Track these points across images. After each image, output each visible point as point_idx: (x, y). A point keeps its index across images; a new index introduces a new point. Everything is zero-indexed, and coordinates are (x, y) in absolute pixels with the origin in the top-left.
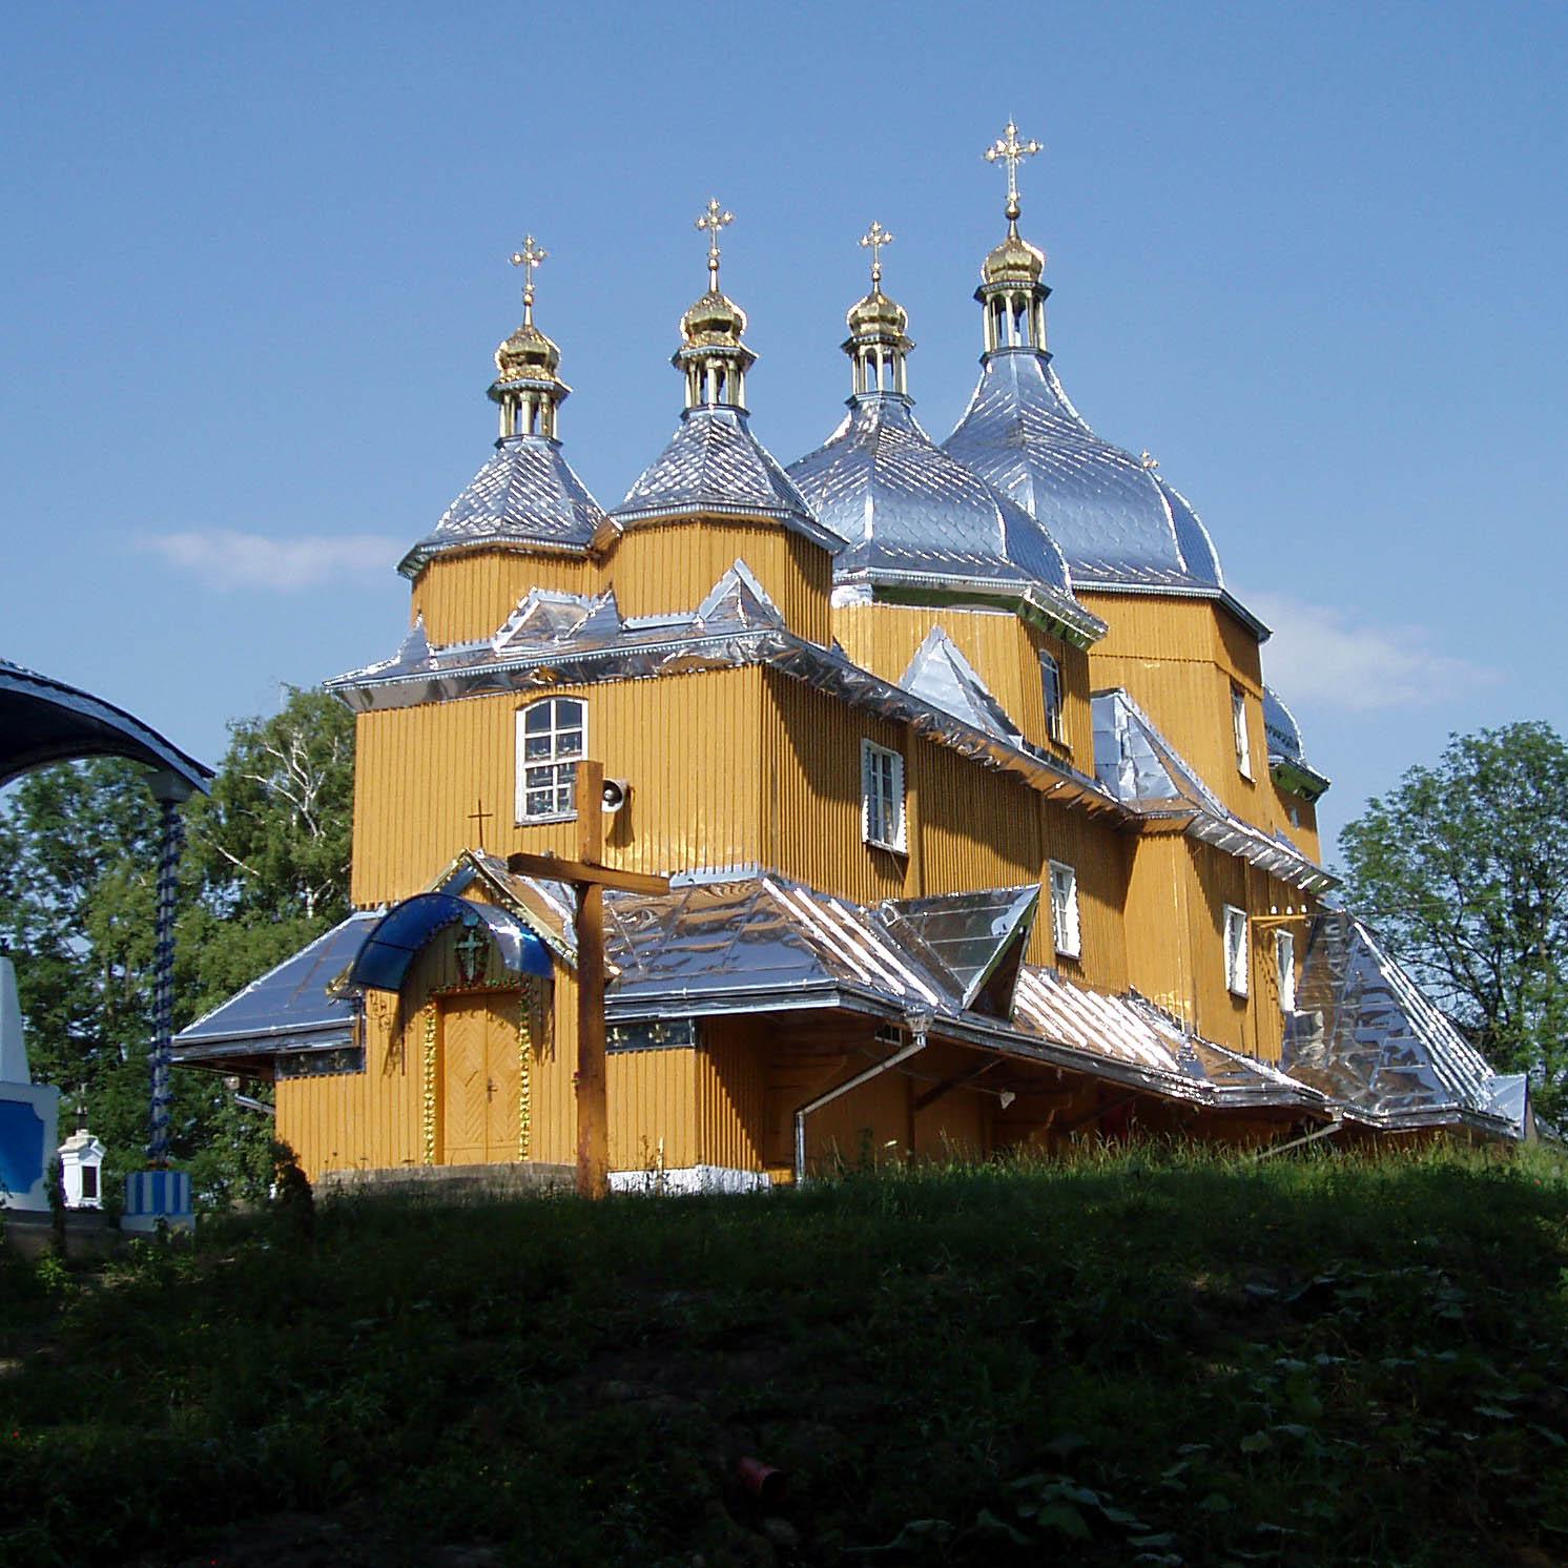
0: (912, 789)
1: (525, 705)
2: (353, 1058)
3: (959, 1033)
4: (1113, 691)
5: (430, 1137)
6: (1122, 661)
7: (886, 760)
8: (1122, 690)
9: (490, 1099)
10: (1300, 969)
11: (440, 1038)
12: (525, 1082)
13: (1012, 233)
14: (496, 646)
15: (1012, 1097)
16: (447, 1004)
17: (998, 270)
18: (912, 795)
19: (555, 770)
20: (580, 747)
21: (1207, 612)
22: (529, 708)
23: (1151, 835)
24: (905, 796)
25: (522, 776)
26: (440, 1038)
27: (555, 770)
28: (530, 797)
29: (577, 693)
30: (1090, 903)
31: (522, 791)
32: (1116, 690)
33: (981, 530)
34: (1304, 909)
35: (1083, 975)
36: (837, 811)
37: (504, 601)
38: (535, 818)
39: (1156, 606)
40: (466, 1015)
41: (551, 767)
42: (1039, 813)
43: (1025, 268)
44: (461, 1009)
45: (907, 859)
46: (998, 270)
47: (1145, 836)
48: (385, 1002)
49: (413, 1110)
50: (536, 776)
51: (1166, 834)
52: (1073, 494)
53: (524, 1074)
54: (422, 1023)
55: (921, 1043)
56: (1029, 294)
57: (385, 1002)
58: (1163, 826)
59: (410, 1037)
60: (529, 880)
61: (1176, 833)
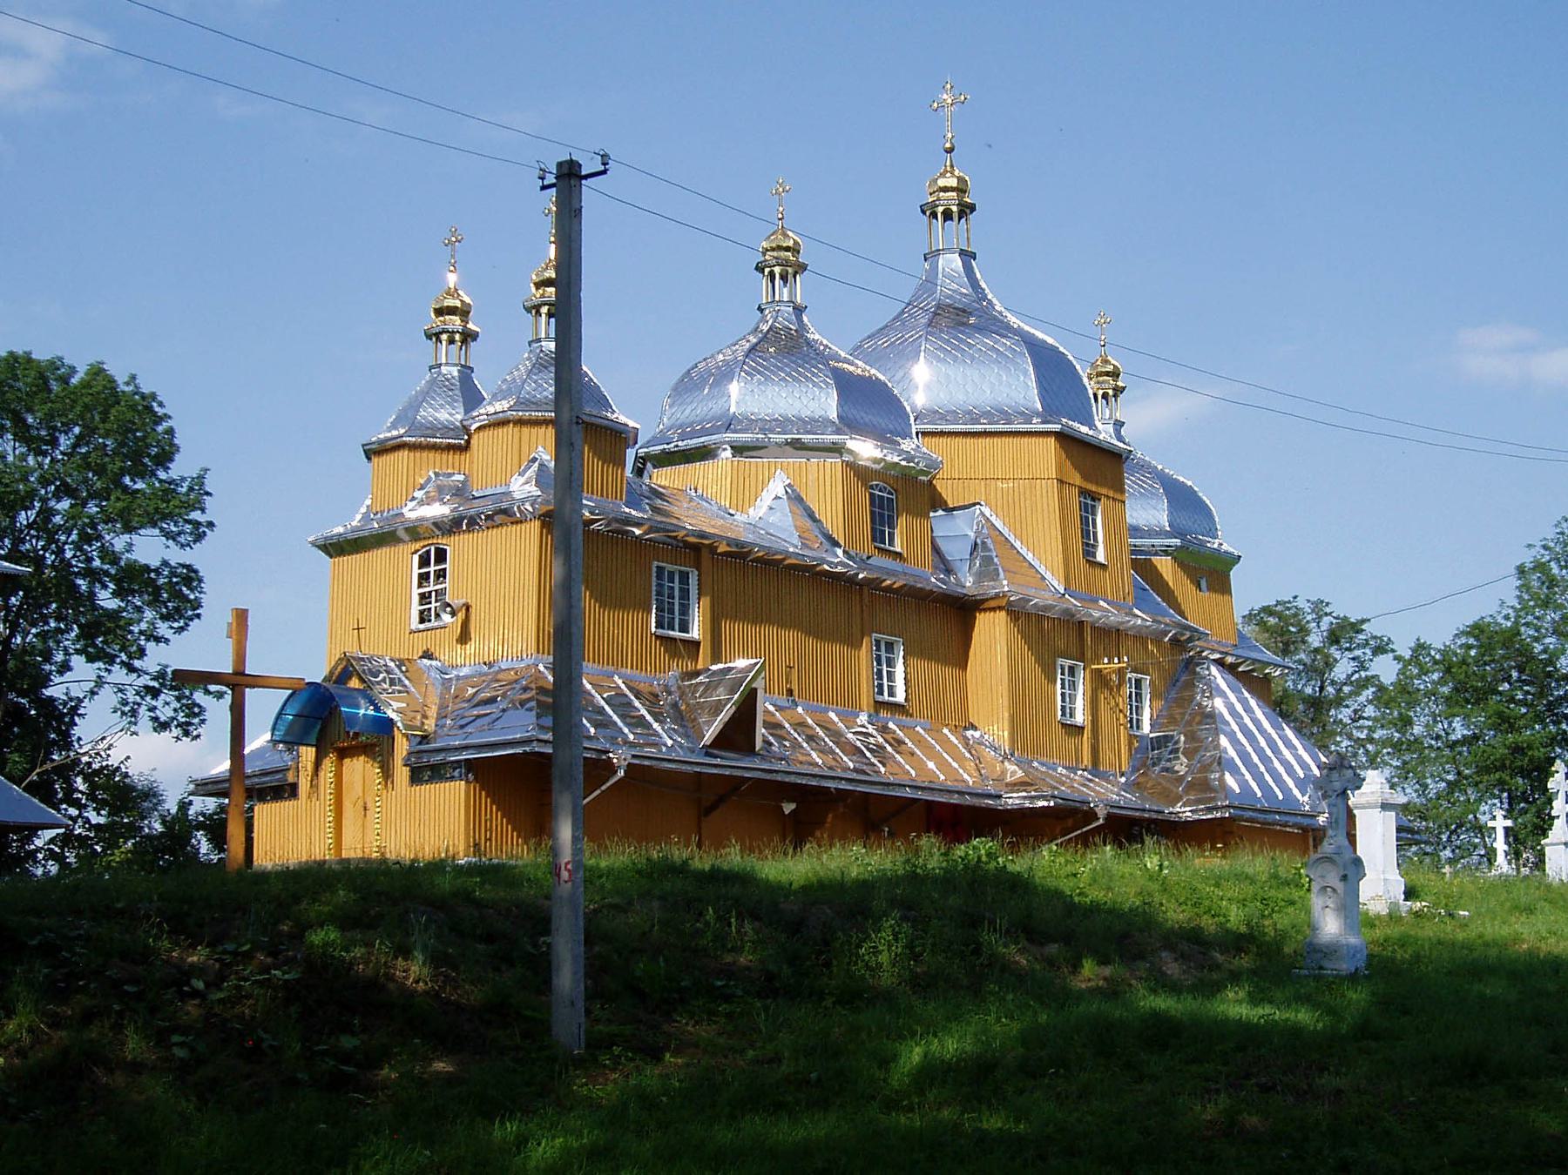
0: (706, 595)
1: (418, 550)
2: (291, 791)
3: (654, 763)
4: (974, 504)
5: (330, 841)
6: (983, 482)
7: (684, 578)
8: (982, 503)
9: (365, 815)
10: (1159, 704)
11: (339, 776)
12: (378, 804)
13: (948, 164)
14: (405, 510)
15: (793, 806)
16: (343, 754)
17: (934, 192)
18: (706, 601)
19: (433, 594)
20: (445, 578)
21: (1052, 441)
22: (420, 553)
23: (985, 610)
24: (699, 599)
25: (416, 599)
26: (339, 776)
27: (433, 594)
28: (421, 612)
29: (444, 542)
30: (921, 666)
31: (416, 608)
32: (979, 504)
33: (819, 400)
34: (1126, 659)
35: (911, 716)
36: (630, 617)
37: (411, 480)
38: (422, 627)
39: (1010, 440)
40: (355, 760)
41: (430, 592)
42: (861, 600)
43: (787, 249)
44: (352, 756)
45: (699, 643)
46: (934, 192)
47: (981, 611)
48: (308, 753)
49: (322, 826)
50: (424, 598)
51: (993, 609)
52: (955, 359)
53: (377, 799)
54: (328, 764)
55: (621, 773)
56: (955, 209)
57: (308, 753)
58: (992, 604)
59: (322, 774)
60: (1171, 584)
61: (1000, 608)
